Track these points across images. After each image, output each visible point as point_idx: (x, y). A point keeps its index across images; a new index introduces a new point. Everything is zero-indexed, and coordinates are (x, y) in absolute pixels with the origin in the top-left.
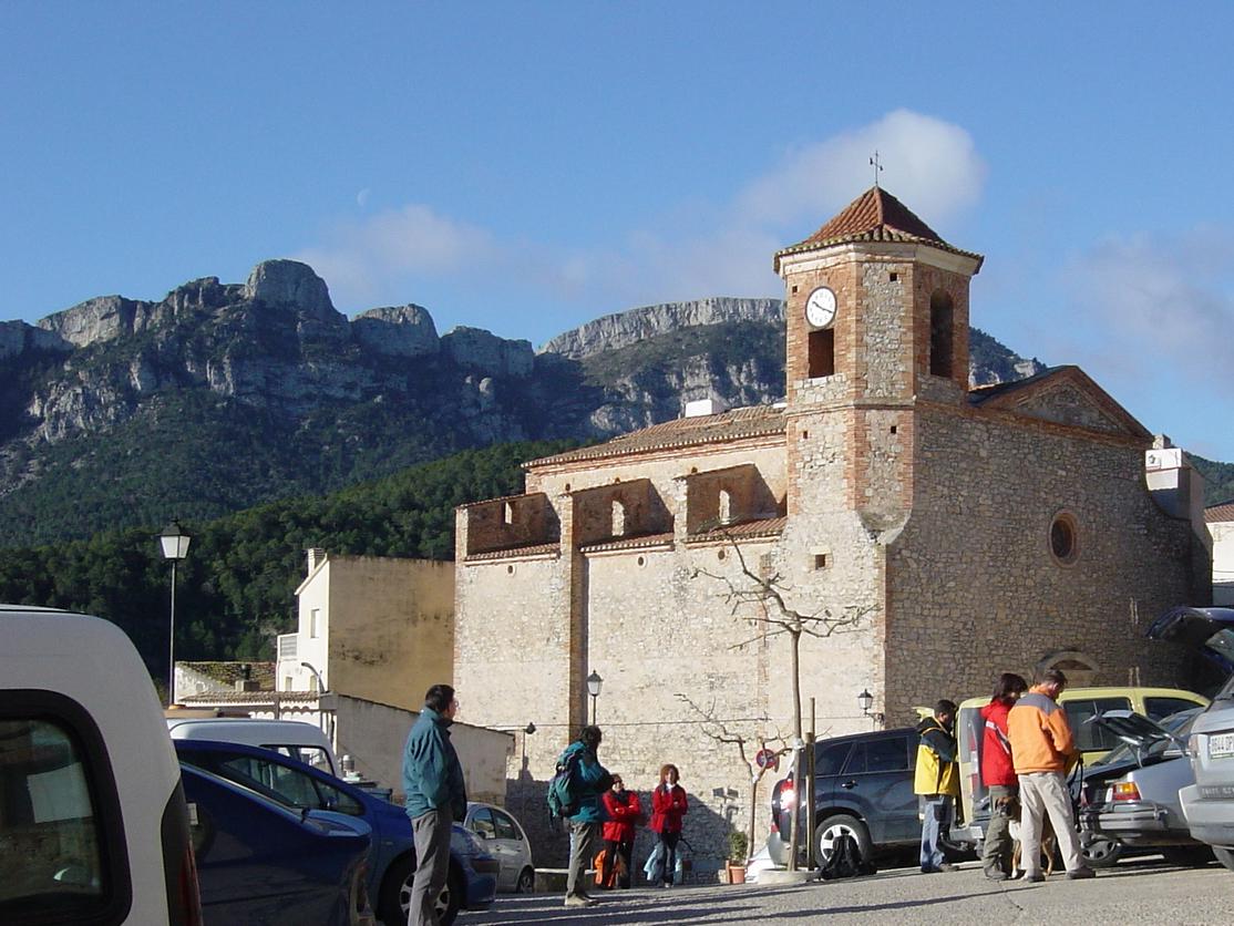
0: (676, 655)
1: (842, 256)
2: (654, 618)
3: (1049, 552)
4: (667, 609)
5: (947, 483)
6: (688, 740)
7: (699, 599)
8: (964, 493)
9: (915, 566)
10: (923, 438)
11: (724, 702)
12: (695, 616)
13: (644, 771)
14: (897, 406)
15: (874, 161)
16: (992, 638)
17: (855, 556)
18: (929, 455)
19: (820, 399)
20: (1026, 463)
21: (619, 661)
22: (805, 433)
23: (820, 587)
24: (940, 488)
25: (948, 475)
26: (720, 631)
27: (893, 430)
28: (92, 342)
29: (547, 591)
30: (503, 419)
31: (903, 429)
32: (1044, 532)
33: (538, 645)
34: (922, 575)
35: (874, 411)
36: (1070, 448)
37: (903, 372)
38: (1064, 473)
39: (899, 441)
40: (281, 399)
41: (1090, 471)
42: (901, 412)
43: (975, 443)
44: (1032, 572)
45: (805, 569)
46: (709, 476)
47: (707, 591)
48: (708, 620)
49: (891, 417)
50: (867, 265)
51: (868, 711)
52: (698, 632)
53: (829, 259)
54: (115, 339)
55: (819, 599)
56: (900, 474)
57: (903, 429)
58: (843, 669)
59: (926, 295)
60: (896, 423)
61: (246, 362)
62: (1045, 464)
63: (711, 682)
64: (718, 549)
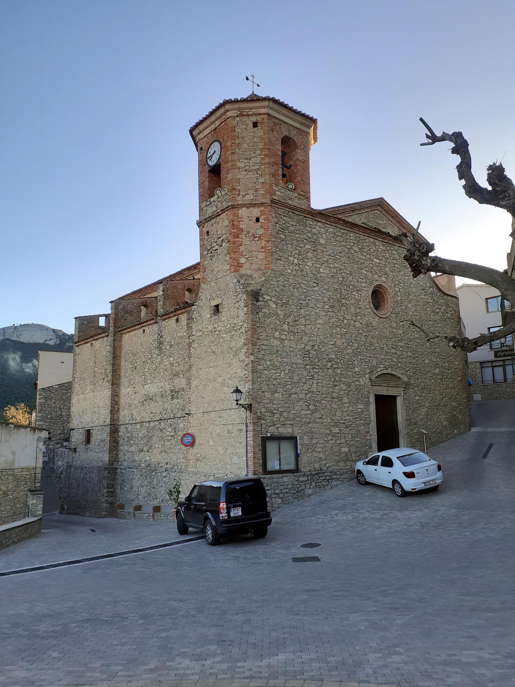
0: (158, 381)
2: (149, 361)
3: (370, 307)
4: (155, 356)
5: (296, 256)
6: (162, 431)
7: (168, 347)
8: (309, 264)
9: (274, 306)
11: (178, 406)
12: (166, 357)
13: (143, 450)
14: (259, 204)
16: (333, 356)
17: (234, 301)
19: (214, 209)
20: (352, 251)
21: (134, 388)
22: (208, 232)
23: (216, 326)
24: (291, 259)
25: (298, 251)
26: (176, 365)
27: (258, 220)
29: (104, 353)
31: (264, 219)
32: (367, 293)
33: (100, 382)
34: (279, 312)
37: (263, 183)
38: (378, 261)
39: (261, 227)
41: (395, 262)
42: (262, 208)
43: (315, 234)
44: (359, 317)
45: (209, 316)
47: (171, 342)
48: (171, 359)
49: (256, 212)
50: (238, 119)
51: (239, 402)
52: (167, 366)
55: (216, 333)
56: (262, 248)
57: (264, 219)
58: (229, 376)
60: (259, 215)
62: (365, 254)
63: (173, 395)
64: (175, 318)
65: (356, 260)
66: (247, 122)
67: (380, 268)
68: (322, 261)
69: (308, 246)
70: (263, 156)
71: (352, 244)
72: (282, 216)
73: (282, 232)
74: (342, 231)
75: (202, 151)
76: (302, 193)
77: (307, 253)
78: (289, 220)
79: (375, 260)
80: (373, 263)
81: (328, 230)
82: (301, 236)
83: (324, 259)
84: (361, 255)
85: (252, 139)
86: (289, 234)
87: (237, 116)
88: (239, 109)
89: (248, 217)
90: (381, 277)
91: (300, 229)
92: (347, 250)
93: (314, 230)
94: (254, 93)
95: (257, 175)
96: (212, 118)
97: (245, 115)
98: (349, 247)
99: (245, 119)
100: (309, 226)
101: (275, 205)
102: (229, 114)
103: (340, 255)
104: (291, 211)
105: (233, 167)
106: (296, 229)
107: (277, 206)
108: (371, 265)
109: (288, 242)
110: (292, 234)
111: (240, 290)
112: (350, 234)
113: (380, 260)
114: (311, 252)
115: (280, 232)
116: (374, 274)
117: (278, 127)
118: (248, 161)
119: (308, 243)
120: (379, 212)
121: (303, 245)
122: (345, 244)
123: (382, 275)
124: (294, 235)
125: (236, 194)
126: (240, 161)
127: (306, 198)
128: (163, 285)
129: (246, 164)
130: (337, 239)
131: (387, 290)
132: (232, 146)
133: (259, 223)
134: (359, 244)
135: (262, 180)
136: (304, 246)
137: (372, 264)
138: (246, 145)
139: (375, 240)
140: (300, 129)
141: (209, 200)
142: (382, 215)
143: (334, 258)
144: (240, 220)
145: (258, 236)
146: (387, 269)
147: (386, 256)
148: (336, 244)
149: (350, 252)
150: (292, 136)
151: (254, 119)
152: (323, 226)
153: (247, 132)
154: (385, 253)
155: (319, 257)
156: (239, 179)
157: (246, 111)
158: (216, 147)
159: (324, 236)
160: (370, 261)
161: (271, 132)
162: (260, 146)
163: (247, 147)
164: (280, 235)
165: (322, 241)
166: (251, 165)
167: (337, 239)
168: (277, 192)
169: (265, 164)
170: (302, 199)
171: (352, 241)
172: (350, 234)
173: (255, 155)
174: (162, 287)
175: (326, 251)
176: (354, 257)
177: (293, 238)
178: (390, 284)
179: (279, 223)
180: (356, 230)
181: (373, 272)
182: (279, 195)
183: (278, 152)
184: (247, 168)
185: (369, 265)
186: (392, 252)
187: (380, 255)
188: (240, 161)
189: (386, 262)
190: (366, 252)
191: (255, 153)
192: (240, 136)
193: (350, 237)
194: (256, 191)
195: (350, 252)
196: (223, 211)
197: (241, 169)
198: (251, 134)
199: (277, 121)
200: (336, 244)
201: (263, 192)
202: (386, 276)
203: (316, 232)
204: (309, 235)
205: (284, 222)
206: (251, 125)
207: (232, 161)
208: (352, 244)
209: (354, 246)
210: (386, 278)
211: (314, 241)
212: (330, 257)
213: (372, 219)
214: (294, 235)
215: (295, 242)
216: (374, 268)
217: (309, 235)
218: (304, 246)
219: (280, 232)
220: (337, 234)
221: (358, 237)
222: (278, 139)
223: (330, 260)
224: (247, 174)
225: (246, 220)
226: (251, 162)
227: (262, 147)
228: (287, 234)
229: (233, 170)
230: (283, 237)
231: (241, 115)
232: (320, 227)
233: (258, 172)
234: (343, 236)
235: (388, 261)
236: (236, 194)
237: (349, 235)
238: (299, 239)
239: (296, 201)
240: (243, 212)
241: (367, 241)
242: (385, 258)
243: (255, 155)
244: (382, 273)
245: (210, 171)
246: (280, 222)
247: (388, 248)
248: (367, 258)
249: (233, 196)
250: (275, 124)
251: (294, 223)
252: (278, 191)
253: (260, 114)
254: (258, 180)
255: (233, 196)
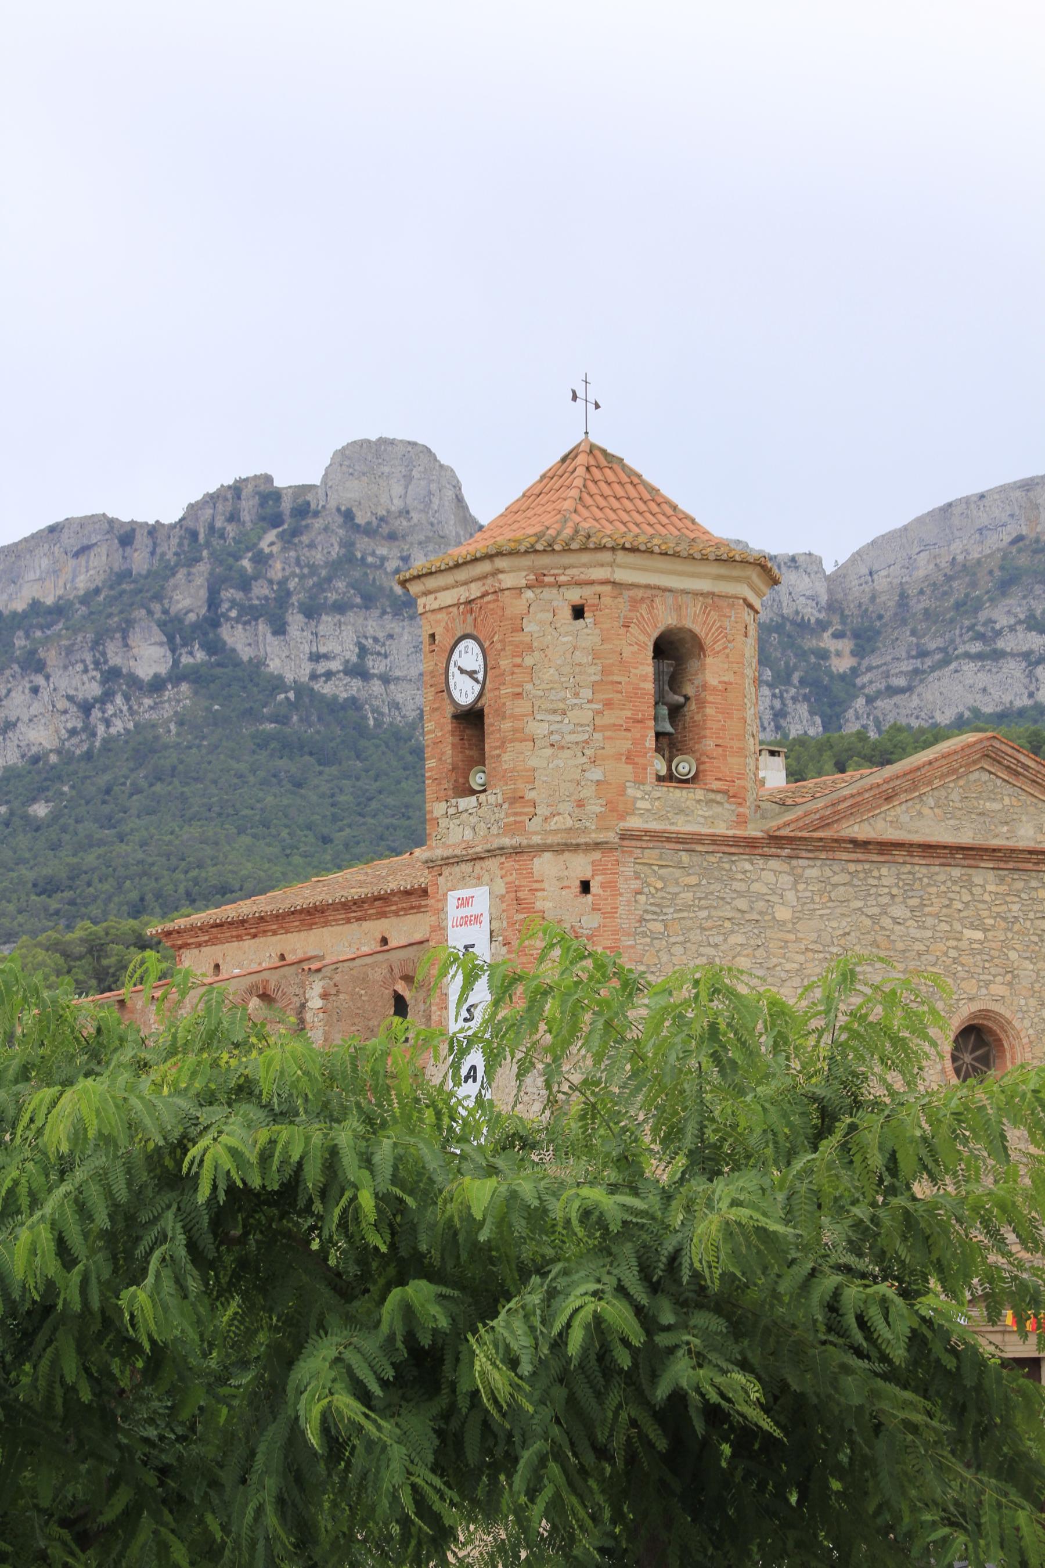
1: (489, 581)
10: (642, 898)
14: (586, 844)
15: (580, 394)
18: (659, 927)
20: (886, 922)
27: (585, 887)
28: (60, 598)
30: (774, 696)
31: (603, 886)
35: (547, 855)
36: (990, 888)
38: (979, 935)
40: (386, 679)
42: (597, 855)
43: (760, 896)
46: (368, 960)
49: (580, 866)
50: (529, 594)
53: (473, 585)
54: (97, 591)
57: (603, 886)
59: (642, 638)
61: (324, 618)
62: (930, 921)
65: (900, 946)
66: (555, 603)
67: (986, 957)
68: (783, 975)
69: (734, 939)
70: (599, 706)
71: (886, 900)
72: (656, 868)
73: (655, 913)
74: (852, 867)
75: (433, 647)
76: (717, 784)
77: (734, 957)
78: (678, 873)
79: (968, 933)
80: (960, 944)
81: (801, 876)
82: (714, 913)
83: (788, 966)
84: (919, 927)
85: (569, 656)
86: (676, 916)
87: (528, 587)
88: (531, 569)
89: (559, 879)
90: (987, 984)
91: (712, 893)
92: (868, 922)
93: (756, 887)
94: (593, 439)
95: (584, 760)
96: (462, 575)
97: (550, 585)
98: (876, 910)
99: (548, 593)
100: (740, 876)
101: (634, 843)
102: (508, 580)
103: (842, 942)
104: (681, 847)
105: (518, 735)
106: (699, 895)
107: (638, 844)
108: (953, 953)
109: (672, 940)
110: (685, 914)
111: (535, 1090)
112: (879, 869)
113: (985, 930)
114: (745, 952)
115: (648, 917)
116: (964, 979)
117: (643, 609)
118: (559, 718)
119: (736, 928)
120: (985, 777)
121: (721, 938)
122: (860, 904)
123: (994, 976)
124: (692, 915)
125: (526, 814)
126: (538, 717)
127: (730, 797)
128: (323, 978)
129: (552, 728)
130: (833, 895)
131: (1009, 1023)
132: (513, 673)
133: (589, 896)
134: (910, 894)
135: (596, 774)
136: (725, 940)
137: (955, 948)
138: (552, 671)
139: (970, 871)
140: (713, 594)
141: (454, 801)
142: (999, 782)
143: (821, 955)
144: (536, 886)
145: (585, 932)
146: (1013, 955)
147: (1010, 911)
148: (828, 911)
149: (877, 927)
150: (688, 624)
151: (575, 596)
152: (786, 867)
153: (556, 635)
154: (1006, 903)
155: (775, 960)
156: (534, 770)
157: (552, 572)
158: (469, 656)
159: (790, 896)
160: (948, 939)
161: (623, 630)
162: (590, 675)
163: (557, 677)
164: (650, 925)
165: (783, 913)
166: (566, 729)
167: (833, 895)
168: (640, 804)
169: (604, 728)
170: (718, 803)
171: (886, 890)
172: (879, 869)
173: (575, 701)
174: (321, 983)
175: (798, 940)
176: (893, 938)
177: (689, 923)
178: (1023, 1002)
179: (646, 890)
180: (899, 855)
181: (962, 974)
182: (648, 810)
183: (642, 685)
184: (555, 738)
185: (946, 954)
186: (1034, 894)
187: (985, 913)
188: (538, 717)
189: (1011, 930)
190: (937, 915)
191: (576, 695)
192: (535, 644)
193: (879, 878)
194: (580, 804)
195: (877, 927)
196: (492, 853)
197: (537, 742)
198: (565, 639)
199: (640, 593)
200: (828, 911)
201: (599, 809)
202: (1009, 977)
203: (765, 890)
204: (742, 904)
205: (660, 885)
206: (568, 613)
207: (514, 717)
208: (886, 900)
209: (894, 903)
210: (1010, 984)
211: (758, 917)
212: (810, 954)
213: (959, 805)
214: (692, 915)
215: (696, 936)
216: (964, 959)
217: (742, 904)
218: (725, 940)
219: (648, 917)
220: (835, 879)
221: (909, 873)
222: (642, 646)
223: (808, 965)
224: (554, 756)
225: (551, 887)
226: (566, 721)
227: (597, 678)
228: (670, 917)
229: (517, 744)
230: (659, 927)
231: (538, 583)
232: (775, 871)
233: (586, 751)
234: (856, 882)
235: (1016, 927)
236: (526, 814)
237: (876, 873)
238: (709, 924)
239: (700, 812)
240: (545, 865)
241: (942, 877)
242: (1004, 919)
243: (575, 701)
244: (993, 971)
245: (456, 717)
246: (649, 885)
247: (1020, 885)
248: (938, 935)
249: (518, 819)
250: (635, 603)
251: (693, 880)
252: (643, 798)
253: (592, 583)
254: (586, 774)
255: (518, 819)
